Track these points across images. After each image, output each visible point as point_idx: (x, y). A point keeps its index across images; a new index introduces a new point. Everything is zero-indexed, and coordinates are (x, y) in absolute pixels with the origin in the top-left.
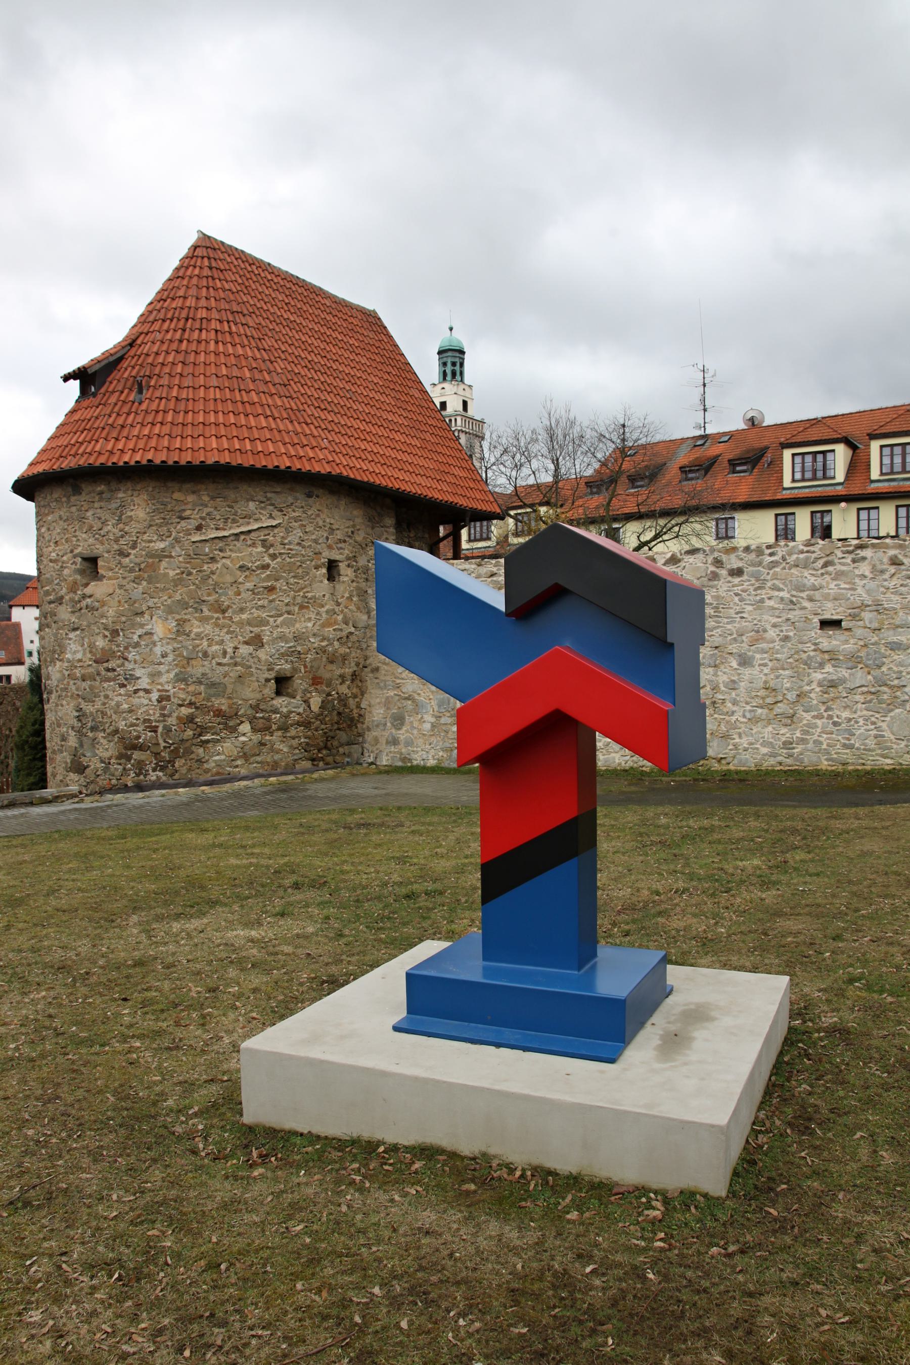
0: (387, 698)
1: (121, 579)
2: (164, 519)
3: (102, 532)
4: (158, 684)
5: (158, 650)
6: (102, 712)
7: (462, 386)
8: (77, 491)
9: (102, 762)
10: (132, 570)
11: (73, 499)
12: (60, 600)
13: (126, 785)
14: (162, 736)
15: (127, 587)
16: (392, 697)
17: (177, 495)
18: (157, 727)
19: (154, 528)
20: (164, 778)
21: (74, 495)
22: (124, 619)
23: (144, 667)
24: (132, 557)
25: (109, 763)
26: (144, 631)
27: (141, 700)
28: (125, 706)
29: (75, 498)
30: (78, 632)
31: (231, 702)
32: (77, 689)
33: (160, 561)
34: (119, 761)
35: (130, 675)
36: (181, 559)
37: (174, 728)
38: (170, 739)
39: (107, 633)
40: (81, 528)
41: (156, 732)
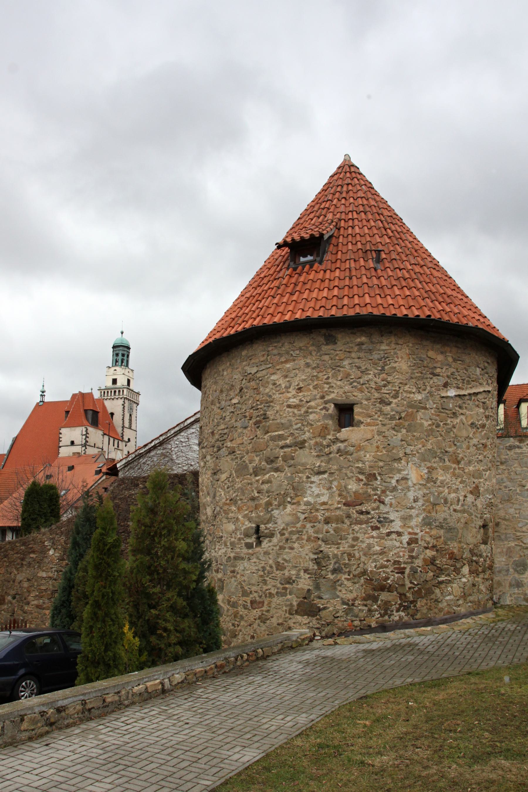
0: (509, 548)
1: (380, 426)
2: (422, 373)
3: (362, 381)
4: (408, 527)
5: (411, 495)
6: (349, 555)
7: (127, 370)
8: (331, 340)
9: (344, 603)
10: (392, 418)
11: (325, 348)
12: (301, 445)
13: (370, 626)
14: (409, 577)
15: (387, 434)
16: (514, 548)
17: (431, 354)
18: (405, 568)
19: (414, 380)
20: (406, 618)
21: (327, 344)
22: (381, 464)
23: (397, 511)
24: (393, 405)
25: (353, 605)
26: (401, 476)
27: (392, 542)
28: (377, 548)
29: (329, 347)
30: (326, 476)
31: (460, 545)
32: (316, 532)
33: (417, 411)
34: (365, 603)
35: (384, 518)
36: (433, 411)
37: (419, 569)
38: (416, 579)
39: (361, 477)
40: (334, 376)
41: (403, 573)
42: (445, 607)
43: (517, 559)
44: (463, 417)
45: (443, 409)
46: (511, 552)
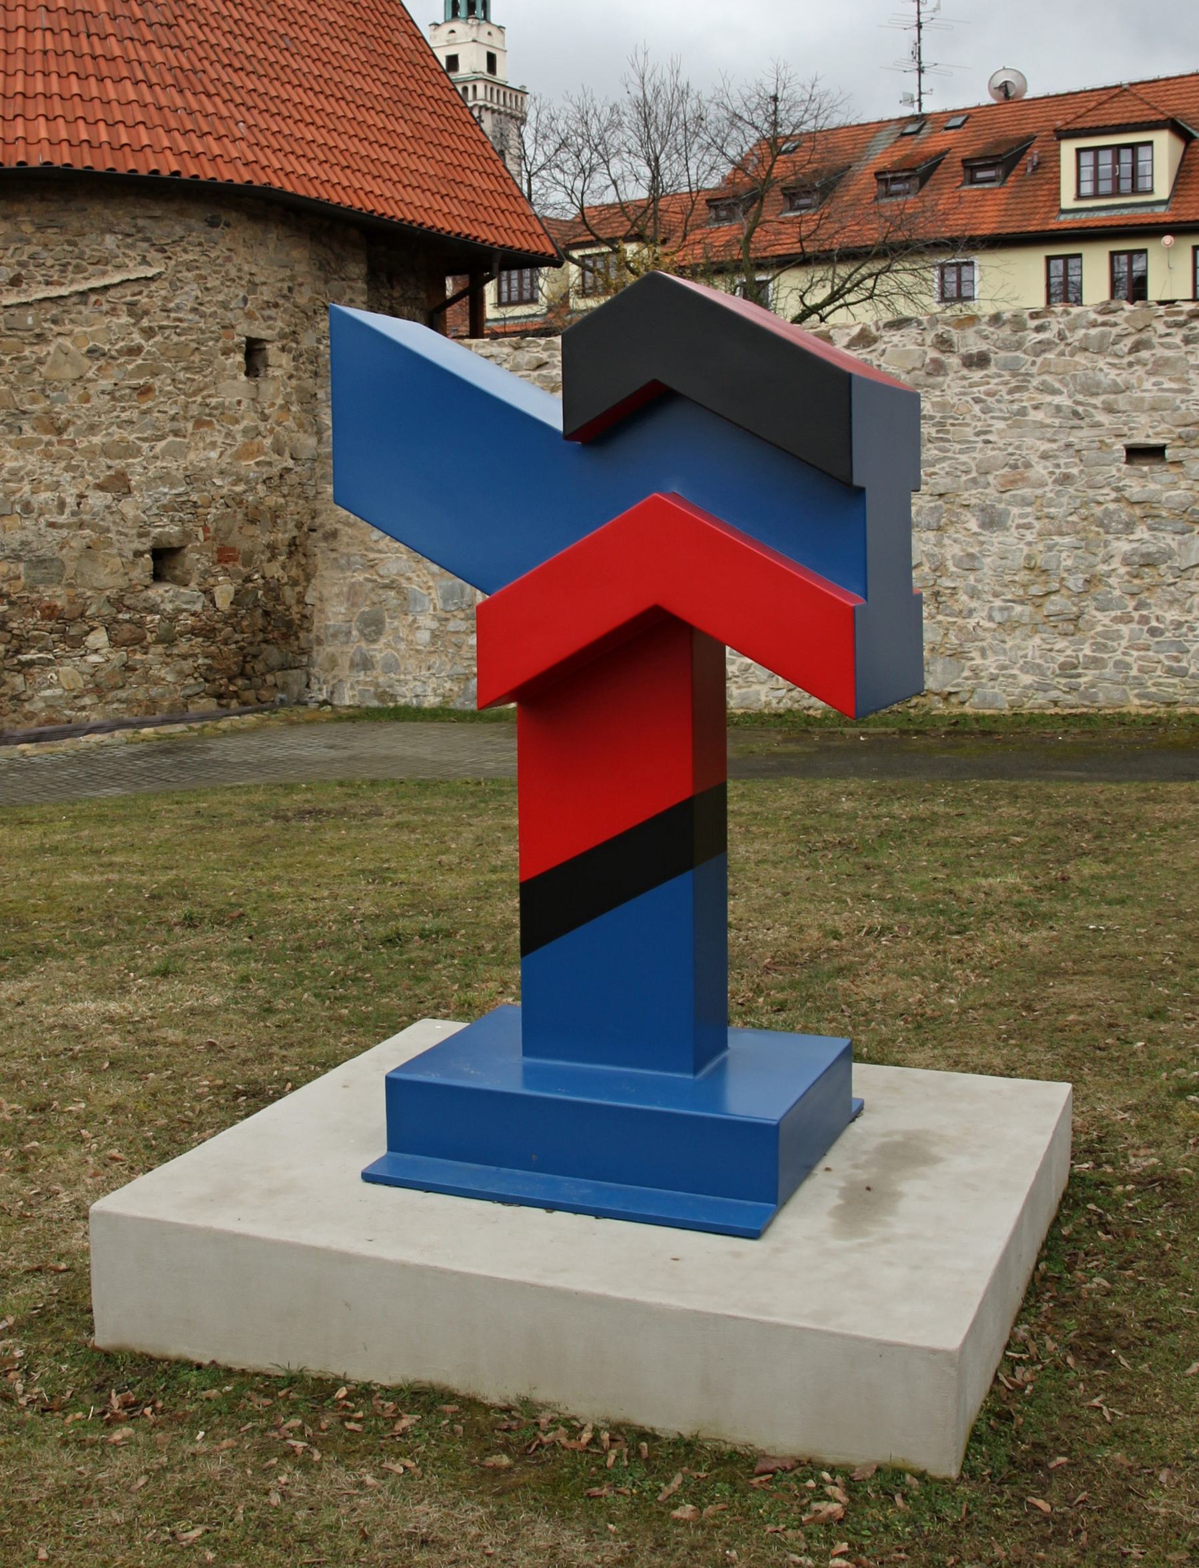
0: (353, 585)
7: (486, 28)
16: (361, 585)
31: (72, 592)
42: (42, 710)
43: (367, 609)
44: (67, 342)
45: (9, 329)
46: (356, 593)
